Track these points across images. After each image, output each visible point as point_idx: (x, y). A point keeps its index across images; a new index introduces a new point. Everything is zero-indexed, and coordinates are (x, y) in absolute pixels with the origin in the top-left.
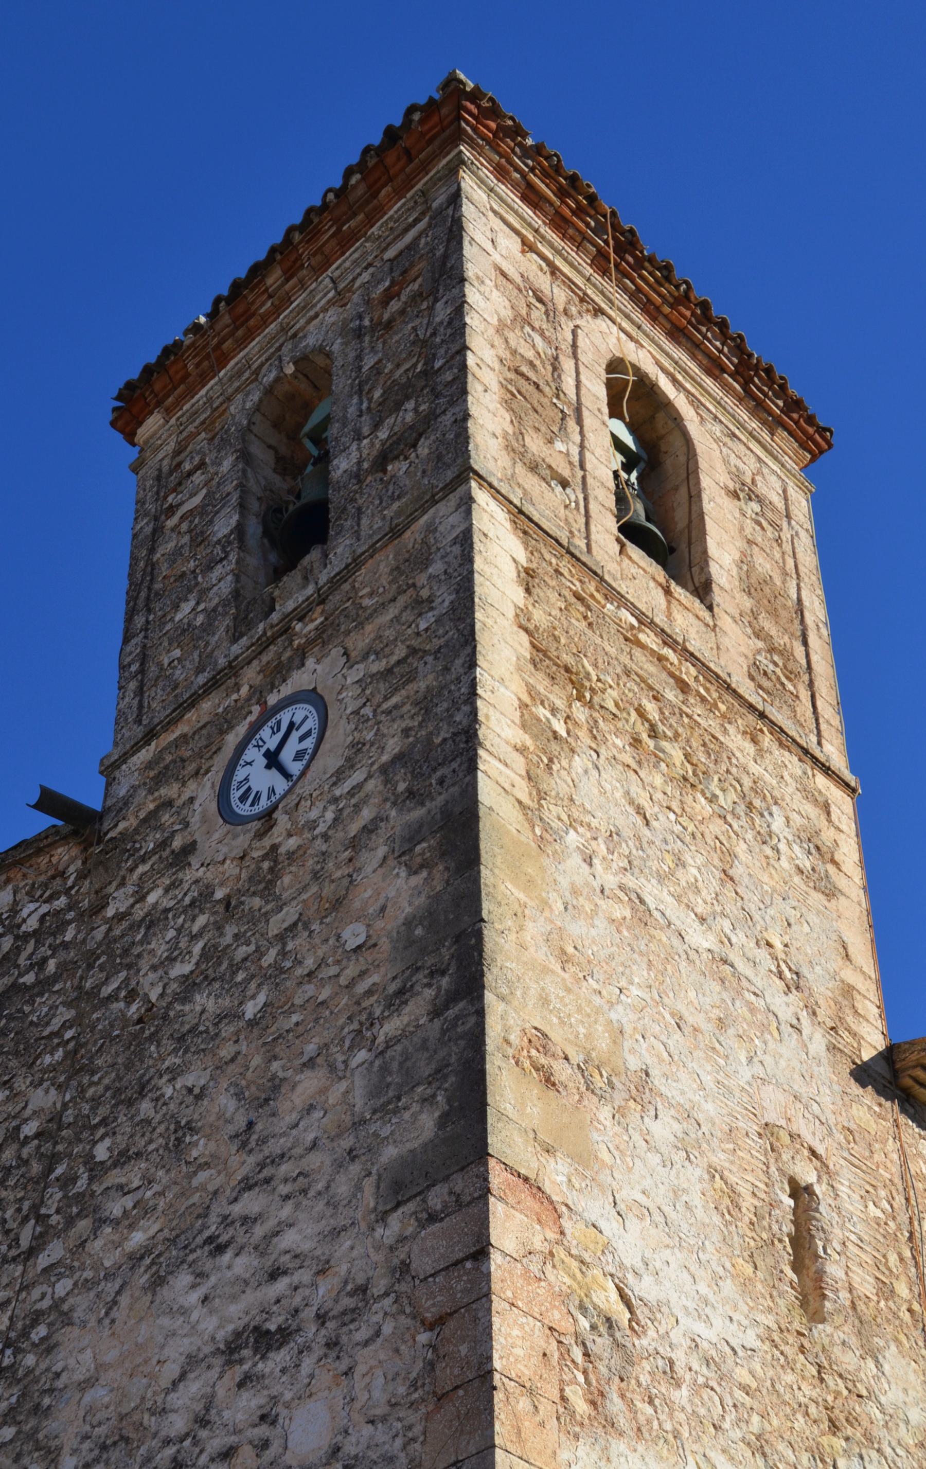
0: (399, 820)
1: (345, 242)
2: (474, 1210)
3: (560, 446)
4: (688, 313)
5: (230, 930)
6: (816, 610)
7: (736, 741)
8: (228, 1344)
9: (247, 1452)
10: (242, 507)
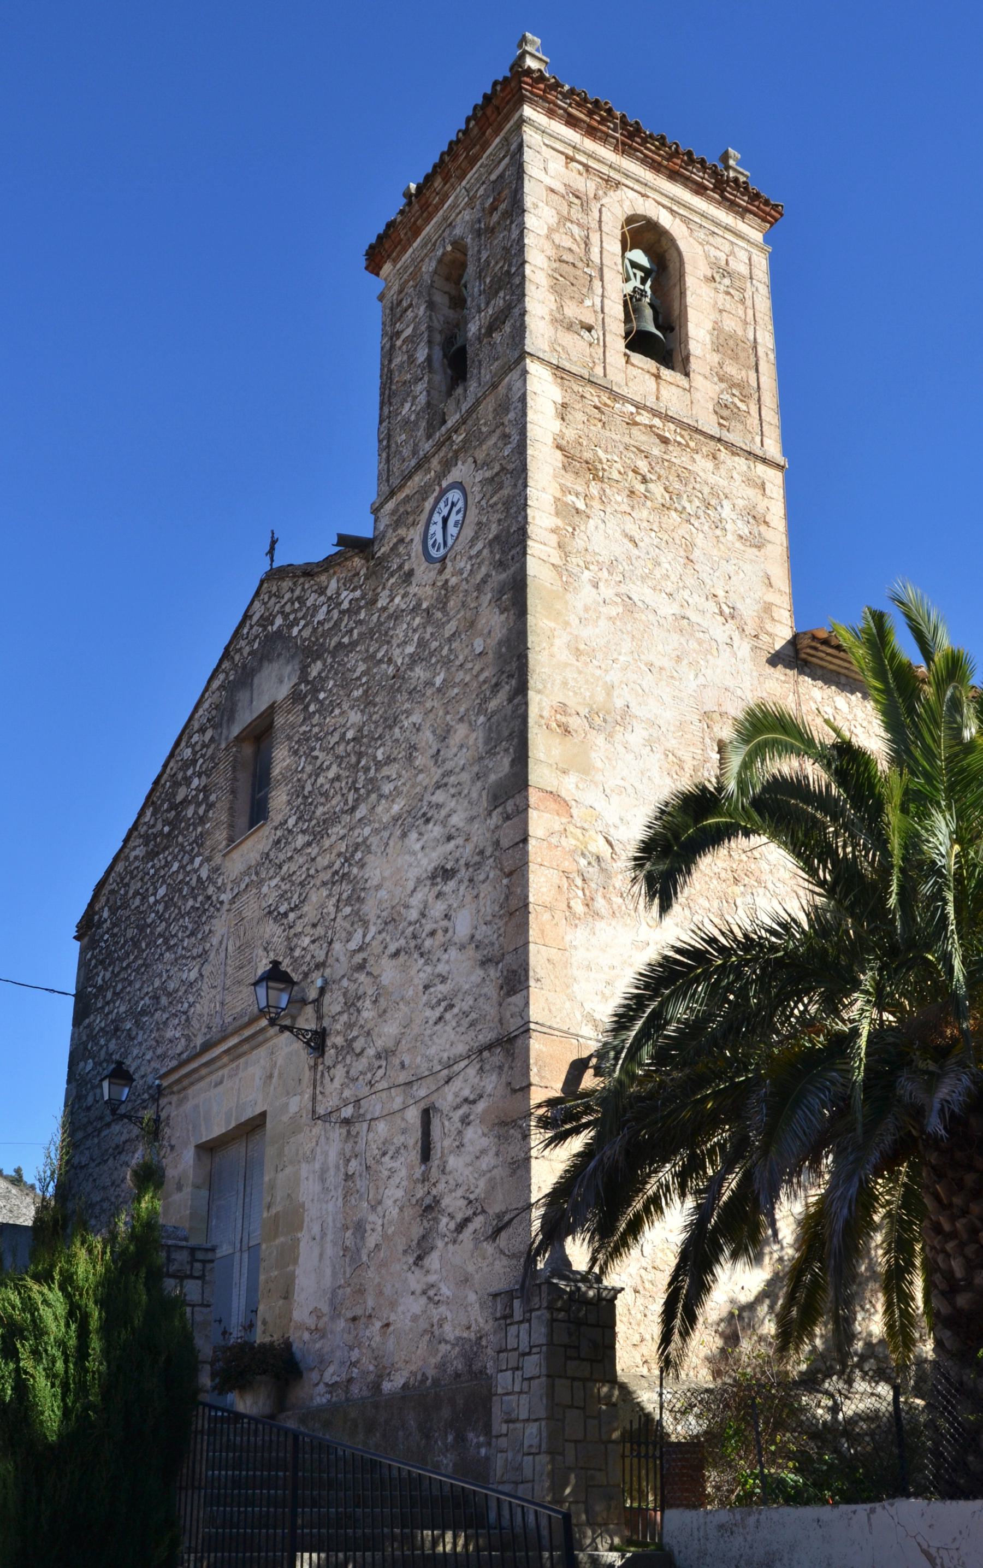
1: (472, 161)
4: (679, 162)
7: (702, 465)
9: (440, 932)
10: (430, 342)
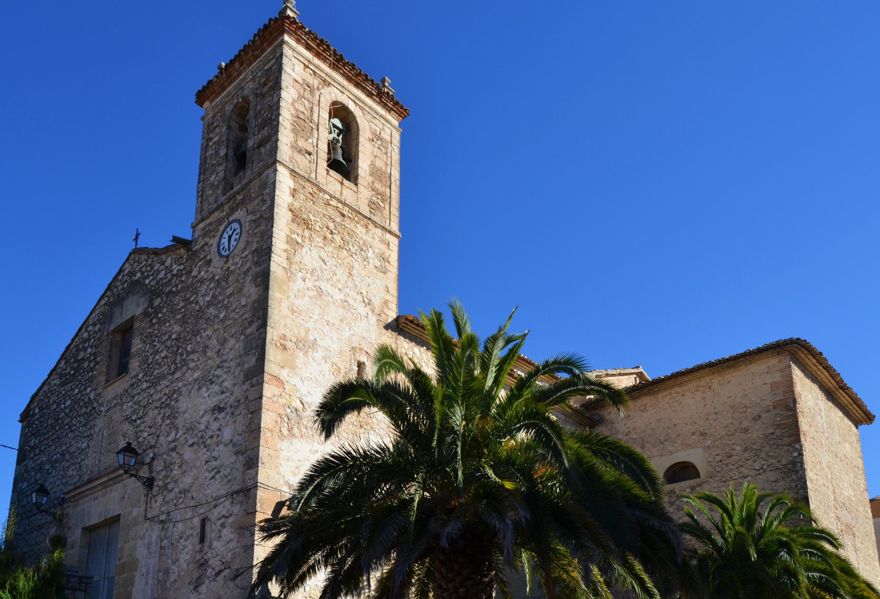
3: (310, 141)
5: (218, 290)
6: (396, 174)
10: (227, 147)
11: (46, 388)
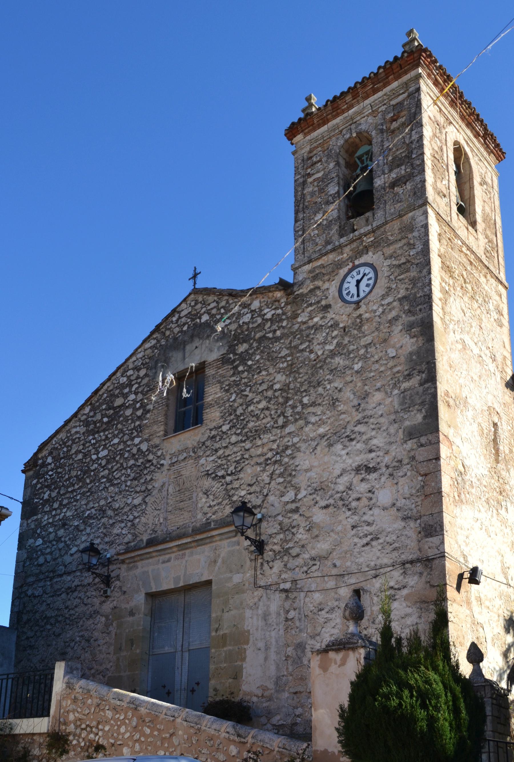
0: (405, 319)
1: (375, 91)
2: (435, 446)
7: (482, 280)
8: (356, 468)
11: (62, 435)
